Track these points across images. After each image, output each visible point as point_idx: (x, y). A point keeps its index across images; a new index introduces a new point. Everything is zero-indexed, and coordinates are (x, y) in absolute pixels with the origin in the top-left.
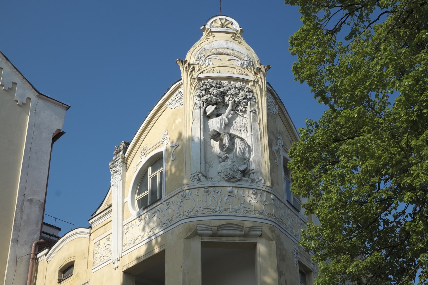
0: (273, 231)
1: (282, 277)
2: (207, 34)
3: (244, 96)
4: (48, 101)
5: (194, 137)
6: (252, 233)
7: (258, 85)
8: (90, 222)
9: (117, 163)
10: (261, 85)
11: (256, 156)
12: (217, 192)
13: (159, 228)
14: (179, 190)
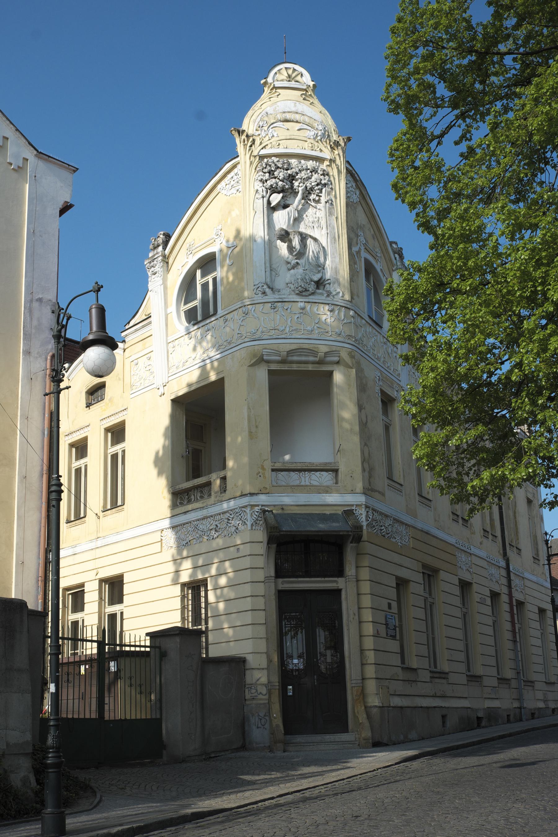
0: (352, 357)
1: (363, 411)
2: (269, 91)
3: (318, 181)
4: (50, 162)
5: (257, 237)
6: (328, 359)
7: (336, 165)
8: (123, 334)
9: (155, 262)
10: (339, 164)
11: (332, 262)
12: (286, 308)
13: (214, 350)
14: (239, 304)
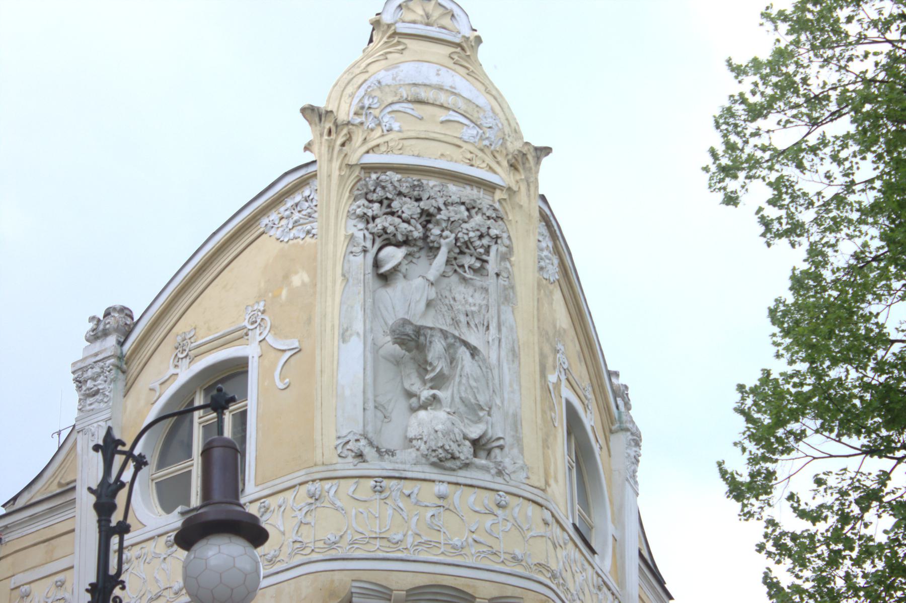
2: (385, 39)
